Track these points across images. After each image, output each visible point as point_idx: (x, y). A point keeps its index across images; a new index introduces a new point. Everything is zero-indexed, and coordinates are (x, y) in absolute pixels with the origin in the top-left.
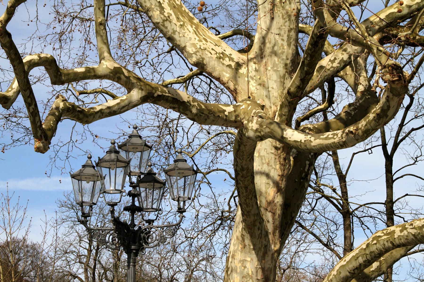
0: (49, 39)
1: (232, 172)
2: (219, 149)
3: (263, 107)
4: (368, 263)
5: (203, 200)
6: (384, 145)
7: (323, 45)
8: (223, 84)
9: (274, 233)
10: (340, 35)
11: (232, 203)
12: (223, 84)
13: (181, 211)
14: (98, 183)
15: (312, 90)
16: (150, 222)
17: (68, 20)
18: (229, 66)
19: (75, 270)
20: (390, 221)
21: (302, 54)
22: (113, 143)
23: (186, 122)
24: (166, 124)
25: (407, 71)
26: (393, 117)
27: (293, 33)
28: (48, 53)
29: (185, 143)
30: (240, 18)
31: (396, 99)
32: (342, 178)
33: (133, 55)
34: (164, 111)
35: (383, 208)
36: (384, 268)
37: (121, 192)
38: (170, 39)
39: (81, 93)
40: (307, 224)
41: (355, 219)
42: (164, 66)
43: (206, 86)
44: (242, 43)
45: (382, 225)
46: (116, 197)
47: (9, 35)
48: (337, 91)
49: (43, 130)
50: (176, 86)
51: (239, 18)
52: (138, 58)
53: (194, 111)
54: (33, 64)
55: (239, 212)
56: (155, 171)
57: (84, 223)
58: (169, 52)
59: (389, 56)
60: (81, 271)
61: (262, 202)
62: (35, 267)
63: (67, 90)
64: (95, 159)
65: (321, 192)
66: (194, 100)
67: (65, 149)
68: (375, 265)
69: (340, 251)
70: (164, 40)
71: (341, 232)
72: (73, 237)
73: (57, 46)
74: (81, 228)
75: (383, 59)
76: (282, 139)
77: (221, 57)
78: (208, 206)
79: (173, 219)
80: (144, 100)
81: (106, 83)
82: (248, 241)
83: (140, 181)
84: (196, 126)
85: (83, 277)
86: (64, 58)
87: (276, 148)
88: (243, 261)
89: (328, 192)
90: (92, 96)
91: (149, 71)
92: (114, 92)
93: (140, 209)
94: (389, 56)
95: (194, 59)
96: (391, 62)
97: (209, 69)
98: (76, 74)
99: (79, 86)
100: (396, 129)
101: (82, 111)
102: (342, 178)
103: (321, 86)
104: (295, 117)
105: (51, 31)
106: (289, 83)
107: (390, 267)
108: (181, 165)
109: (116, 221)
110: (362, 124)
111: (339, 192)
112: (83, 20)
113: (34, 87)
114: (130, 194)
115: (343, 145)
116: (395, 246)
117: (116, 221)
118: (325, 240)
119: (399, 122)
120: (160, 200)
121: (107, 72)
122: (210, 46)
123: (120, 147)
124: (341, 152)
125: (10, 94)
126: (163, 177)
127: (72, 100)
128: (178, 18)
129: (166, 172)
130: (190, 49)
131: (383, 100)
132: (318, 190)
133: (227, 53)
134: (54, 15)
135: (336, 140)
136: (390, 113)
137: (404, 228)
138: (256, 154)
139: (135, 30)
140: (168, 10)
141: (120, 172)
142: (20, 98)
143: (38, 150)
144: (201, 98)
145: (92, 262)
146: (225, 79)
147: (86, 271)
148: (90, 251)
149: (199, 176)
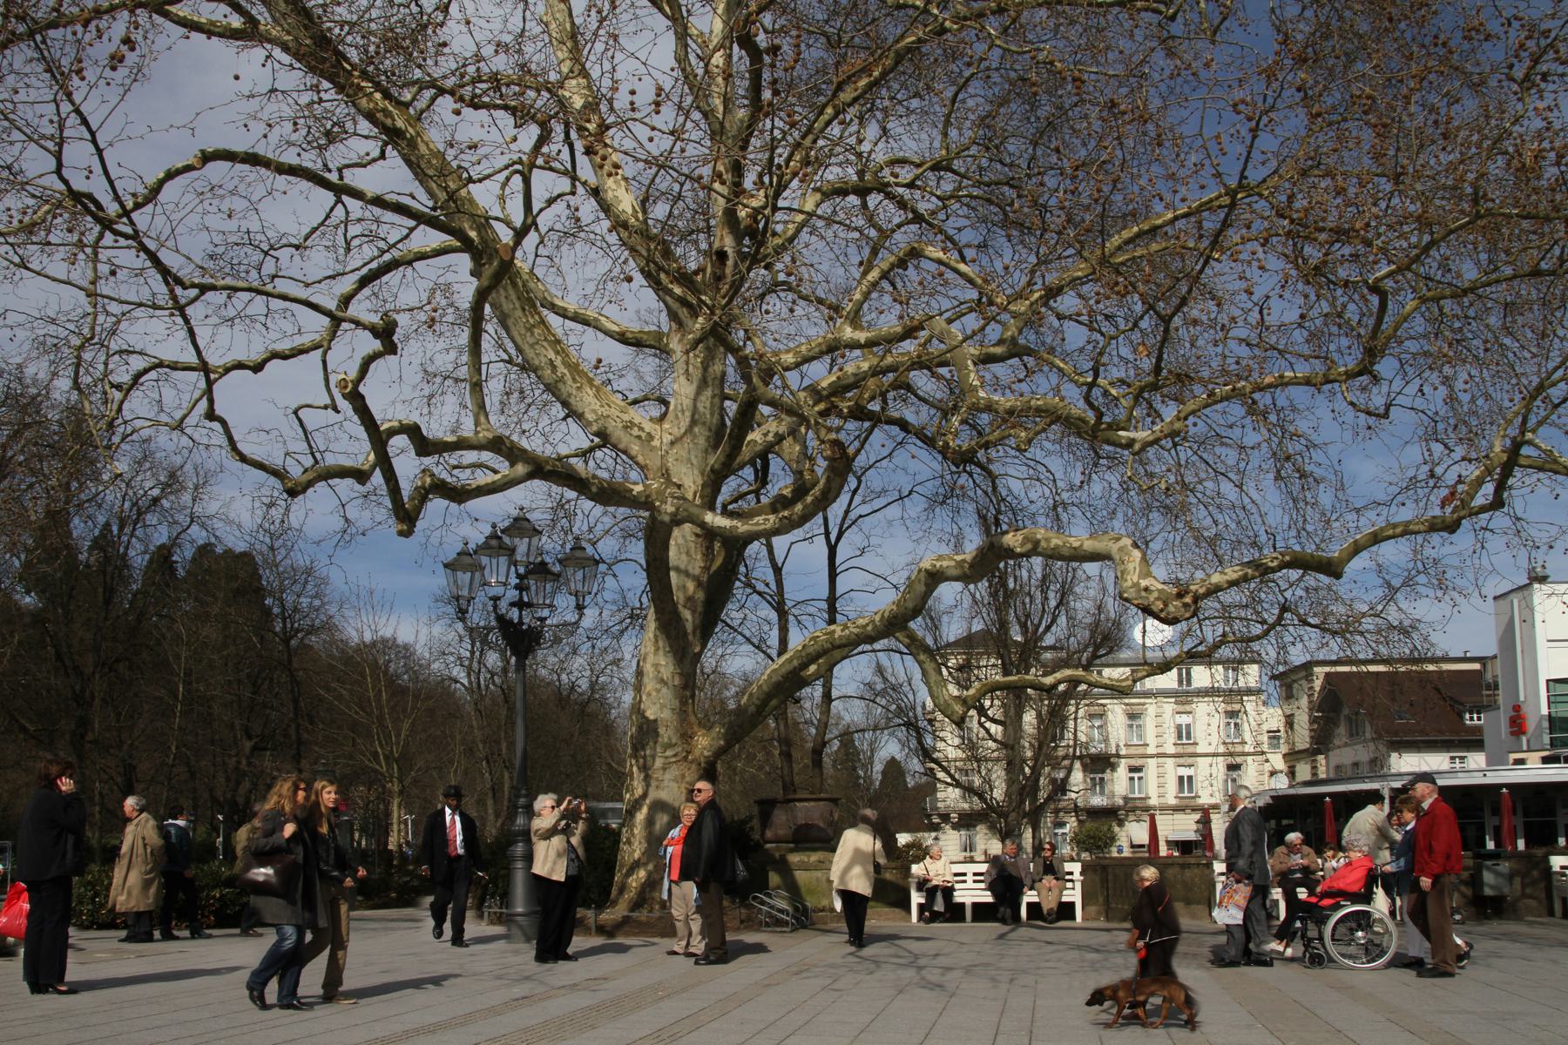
0: (415, 403)
1: (643, 562)
2: (627, 535)
3: (679, 487)
4: (805, 666)
5: (608, 595)
6: (827, 534)
7: (753, 415)
8: (631, 458)
9: (694, 633)
10: (772, 403)
11: (645, 600)
12: (631, 458)
13: (580, 608)
14: (477, 575)
15: (742, 467)
16: (543, 620)
17: (438, 380)
18: (639, 437)
19: (455, 673)
20: (832, 621)
21: (728, 423)
22: (494, 526)
23: (587, 504)
24: (561, 505)
25: (851, 450)
26: (837, 496)
27: (717, 400)
28: (414, 418)
29: (585, 528)
30: (653, 381)
31: (838, 480)
32: (777, 570)
33: (519, 422)
34: (556, 489)
35: (824, 605)
36: (823, 669)
37: (505, 584)
38: (565, 404)
39: (455, 467)
40: (735, 624)
41: (791, 618)
42: (558, 436)
43: (611, 461)
44: (656, 410)
45: (822, 624)
46: (499, 591)
47: (363, 397)
48: (772, 470)
49: (406, 511)
50: (573, 461)
51: (651, 380)
52: (525, 426)
53: (594, 489)
54: (392, 432)
55: (652, 610)
56: (548, 560)
57: (463, 620)
58: (564, 419)
59: (830, 430)
60: (463, 674)
61: (679, 597)
62: (408, 669)
63: (438, 463)
64: (472, 546)
65: (754, 588)
66: (594, 476)
67: (437, 533)
68: (813, 668)
69: (774, 653)
70: (558, 405)
71: (775, 633)
72: (451, 636)
73: (425, 411)
74: (459, 626)
75: (823, 432)
76: (702, 525)
77: (628, 426)
78: (614, 602)
79: (571, 617)
80: (530, 476)
81: (486, 456)
82: (661, 644)
83: (529, 573)
84: (599, 509)
85: (465, 682)
86: (434, 426)
87: (697, 535)
88: (656, 666)
89: (760, 587)
90: (468, 471)
91: (540, 442)
92: (496, 467)
93: (529, 605)
94: (830, 430)
95: (595, 428)
96: (833, 436)
97: (613, 440)
98: (446, 443)
99: (453, 458)
100: (841, 514)
101: (454, 489)
102: (777, 570)
103: (752, 462)
104: (720, 500)
105: (417, 393)
106: (712, 460)
107: (831, 669)
108: (578, 554)
109: (501, 619)
110: (799, 507)
111: (773, 586)
112: (457, 380)
113: (394, 461)
114: (517, 587)
115: (777, 532)
116: (835, 647)
117: (501, 619)
118: (755, 641)
119: (845, 507)
120: (554, 593)
121: (484, 441)
122: (614, 412)
123: (503, 531)
124: (776, 541)
125: (366, 467)
126: (557, 568)
127: (445, 476)
128: (574, 380)
129: (560, 561)
130: (590, 417)
131: (822, 481)
132: (748, 585)
133: (636, 421)
134: (421, 375)
135: (768, 526)
136: (831, 496)
137: (845, 627)
138: (672, 542)
139: (522, 392)
140: (562, 369)
141: (503, 560)
142: (378, 473)
143: (401, 533)
144: (604, 475)
145: (475, 665)
146: (633, 453)
147: (469, 675)
148: (472, 653)
149: (602, 567)
